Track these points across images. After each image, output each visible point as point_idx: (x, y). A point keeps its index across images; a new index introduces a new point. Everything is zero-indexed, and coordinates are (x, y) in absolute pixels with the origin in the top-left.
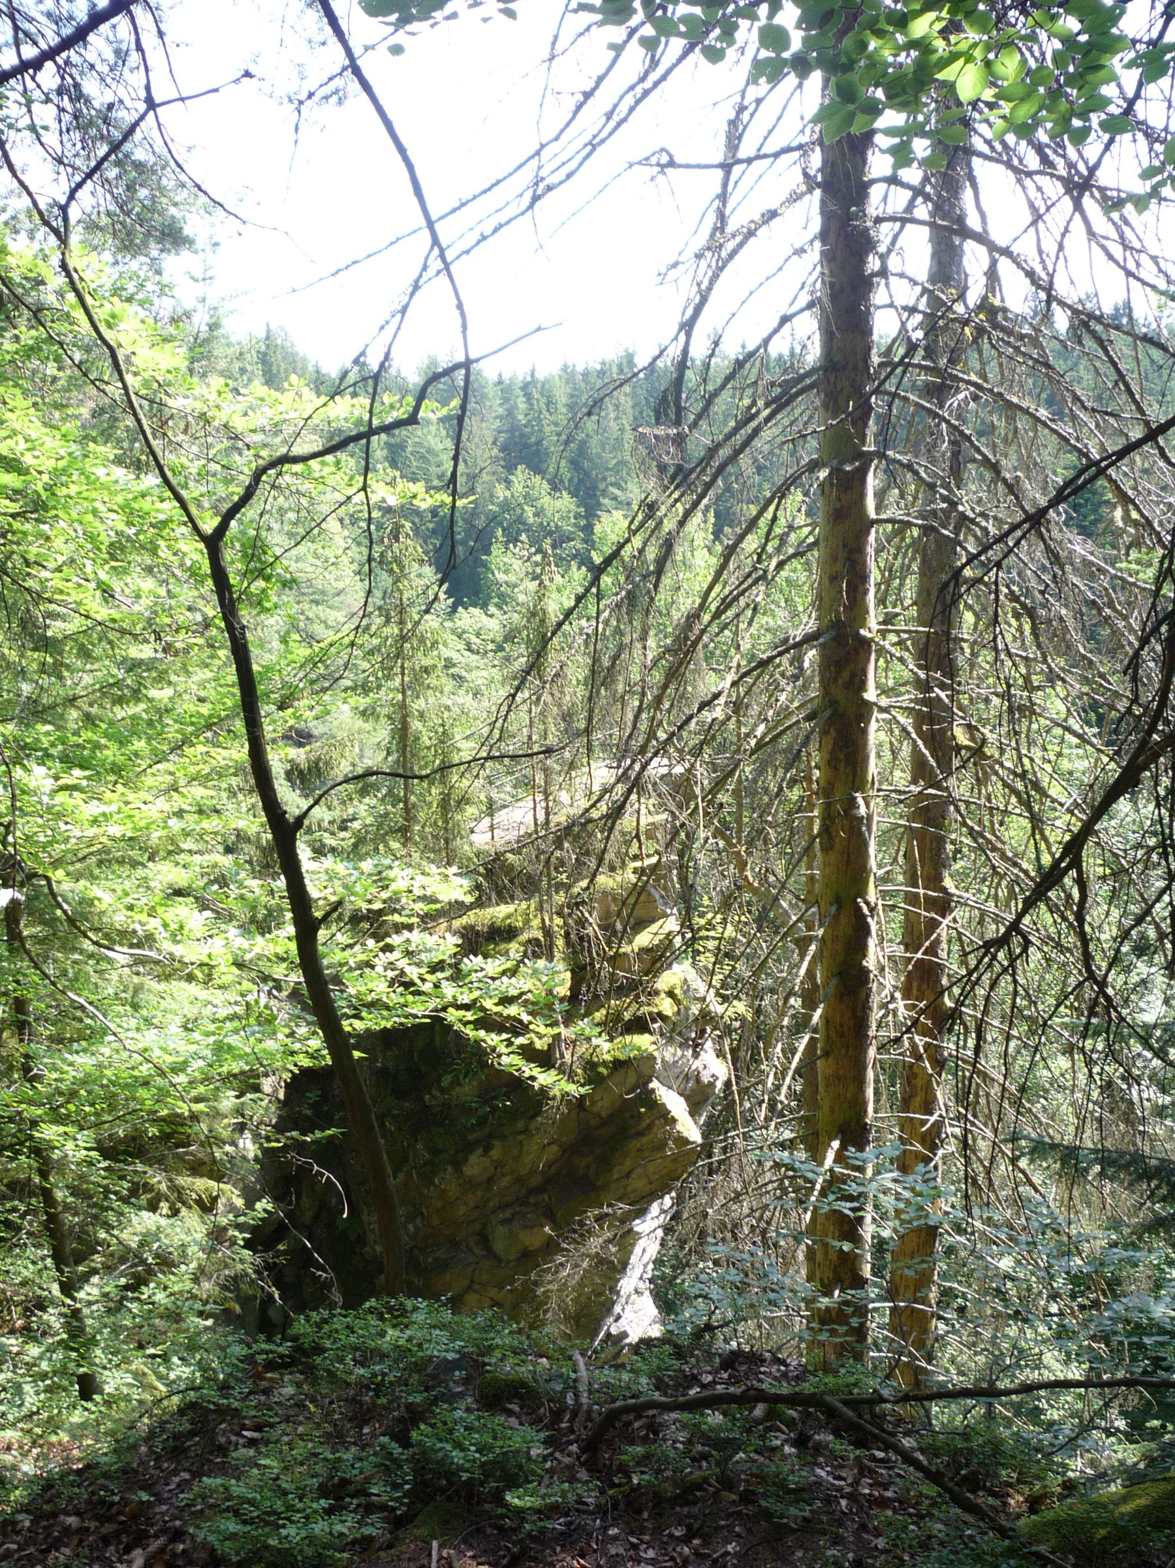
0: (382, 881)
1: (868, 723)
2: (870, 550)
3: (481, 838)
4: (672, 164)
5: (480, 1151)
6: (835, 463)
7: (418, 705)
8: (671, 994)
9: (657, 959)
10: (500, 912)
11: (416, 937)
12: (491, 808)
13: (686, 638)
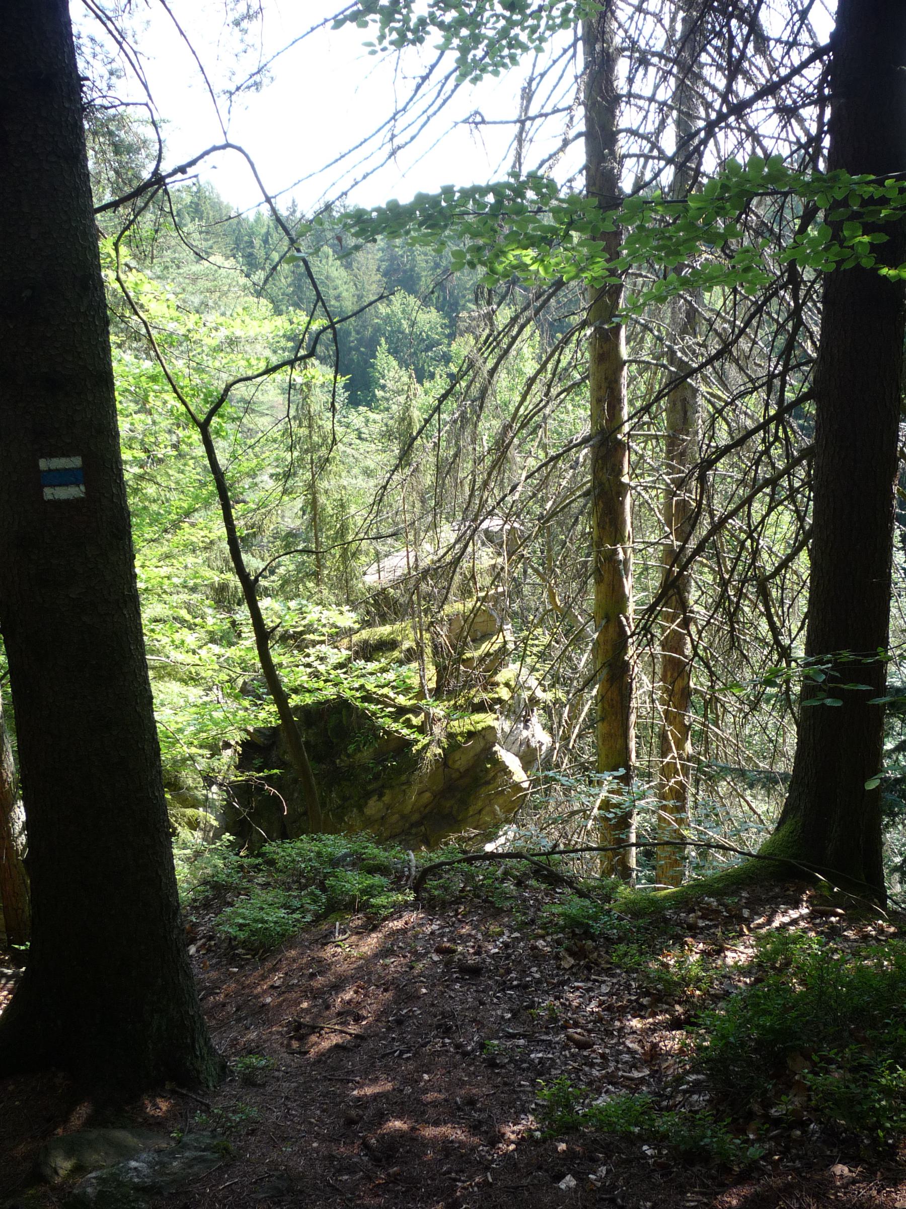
0: (301, 612)
1: (624, 497)
2: (624, 381)
3: (371, 578)
4: (483, 122)
5: (375, 798)
6: (598, 323)
7: (323, 485)
8: (507, 685)
9: (499, 658)
10: (384, 631)
11: (324, 649)
12: (378, 557)
13: (504, 441)
